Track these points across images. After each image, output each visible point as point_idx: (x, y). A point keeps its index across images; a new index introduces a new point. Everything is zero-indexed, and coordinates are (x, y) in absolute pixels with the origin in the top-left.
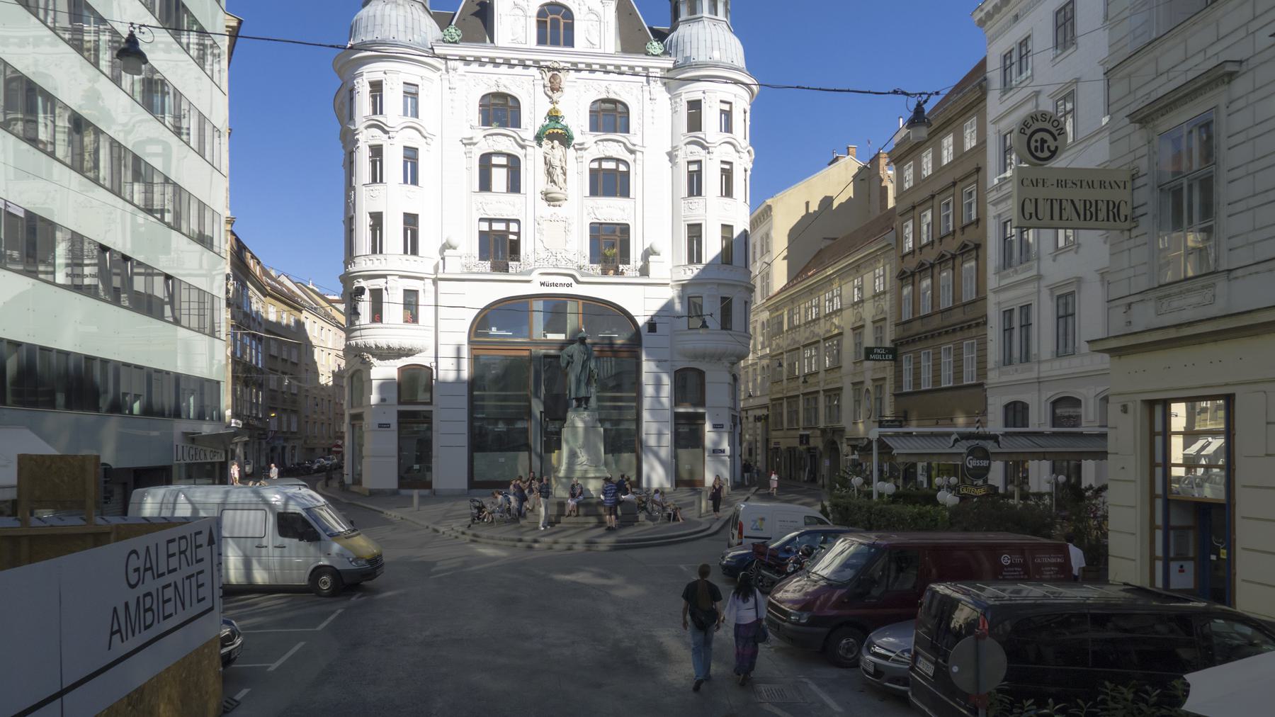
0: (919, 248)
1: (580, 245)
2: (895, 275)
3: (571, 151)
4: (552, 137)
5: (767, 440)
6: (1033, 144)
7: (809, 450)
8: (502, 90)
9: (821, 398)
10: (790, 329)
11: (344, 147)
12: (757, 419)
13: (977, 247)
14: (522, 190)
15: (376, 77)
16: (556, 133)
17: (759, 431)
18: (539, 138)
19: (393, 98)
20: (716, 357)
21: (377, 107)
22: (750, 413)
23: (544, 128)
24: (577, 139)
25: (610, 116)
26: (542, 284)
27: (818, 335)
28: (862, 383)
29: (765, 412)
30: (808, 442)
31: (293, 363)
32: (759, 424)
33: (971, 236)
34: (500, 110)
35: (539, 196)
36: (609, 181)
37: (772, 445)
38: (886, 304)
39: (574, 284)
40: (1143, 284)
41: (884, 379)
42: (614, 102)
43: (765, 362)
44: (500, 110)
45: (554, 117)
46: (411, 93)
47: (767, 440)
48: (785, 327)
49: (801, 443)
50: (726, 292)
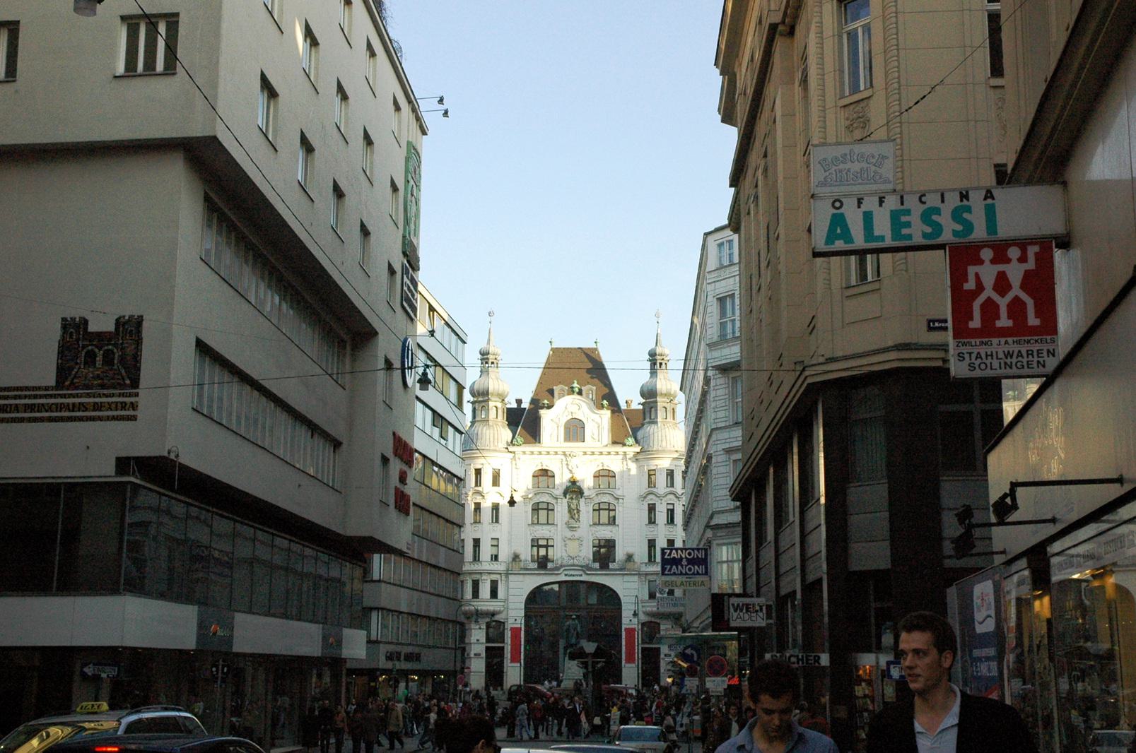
3: (582, 501)
15: (478, 467)
19: (487, 478)
21: (478, 482)
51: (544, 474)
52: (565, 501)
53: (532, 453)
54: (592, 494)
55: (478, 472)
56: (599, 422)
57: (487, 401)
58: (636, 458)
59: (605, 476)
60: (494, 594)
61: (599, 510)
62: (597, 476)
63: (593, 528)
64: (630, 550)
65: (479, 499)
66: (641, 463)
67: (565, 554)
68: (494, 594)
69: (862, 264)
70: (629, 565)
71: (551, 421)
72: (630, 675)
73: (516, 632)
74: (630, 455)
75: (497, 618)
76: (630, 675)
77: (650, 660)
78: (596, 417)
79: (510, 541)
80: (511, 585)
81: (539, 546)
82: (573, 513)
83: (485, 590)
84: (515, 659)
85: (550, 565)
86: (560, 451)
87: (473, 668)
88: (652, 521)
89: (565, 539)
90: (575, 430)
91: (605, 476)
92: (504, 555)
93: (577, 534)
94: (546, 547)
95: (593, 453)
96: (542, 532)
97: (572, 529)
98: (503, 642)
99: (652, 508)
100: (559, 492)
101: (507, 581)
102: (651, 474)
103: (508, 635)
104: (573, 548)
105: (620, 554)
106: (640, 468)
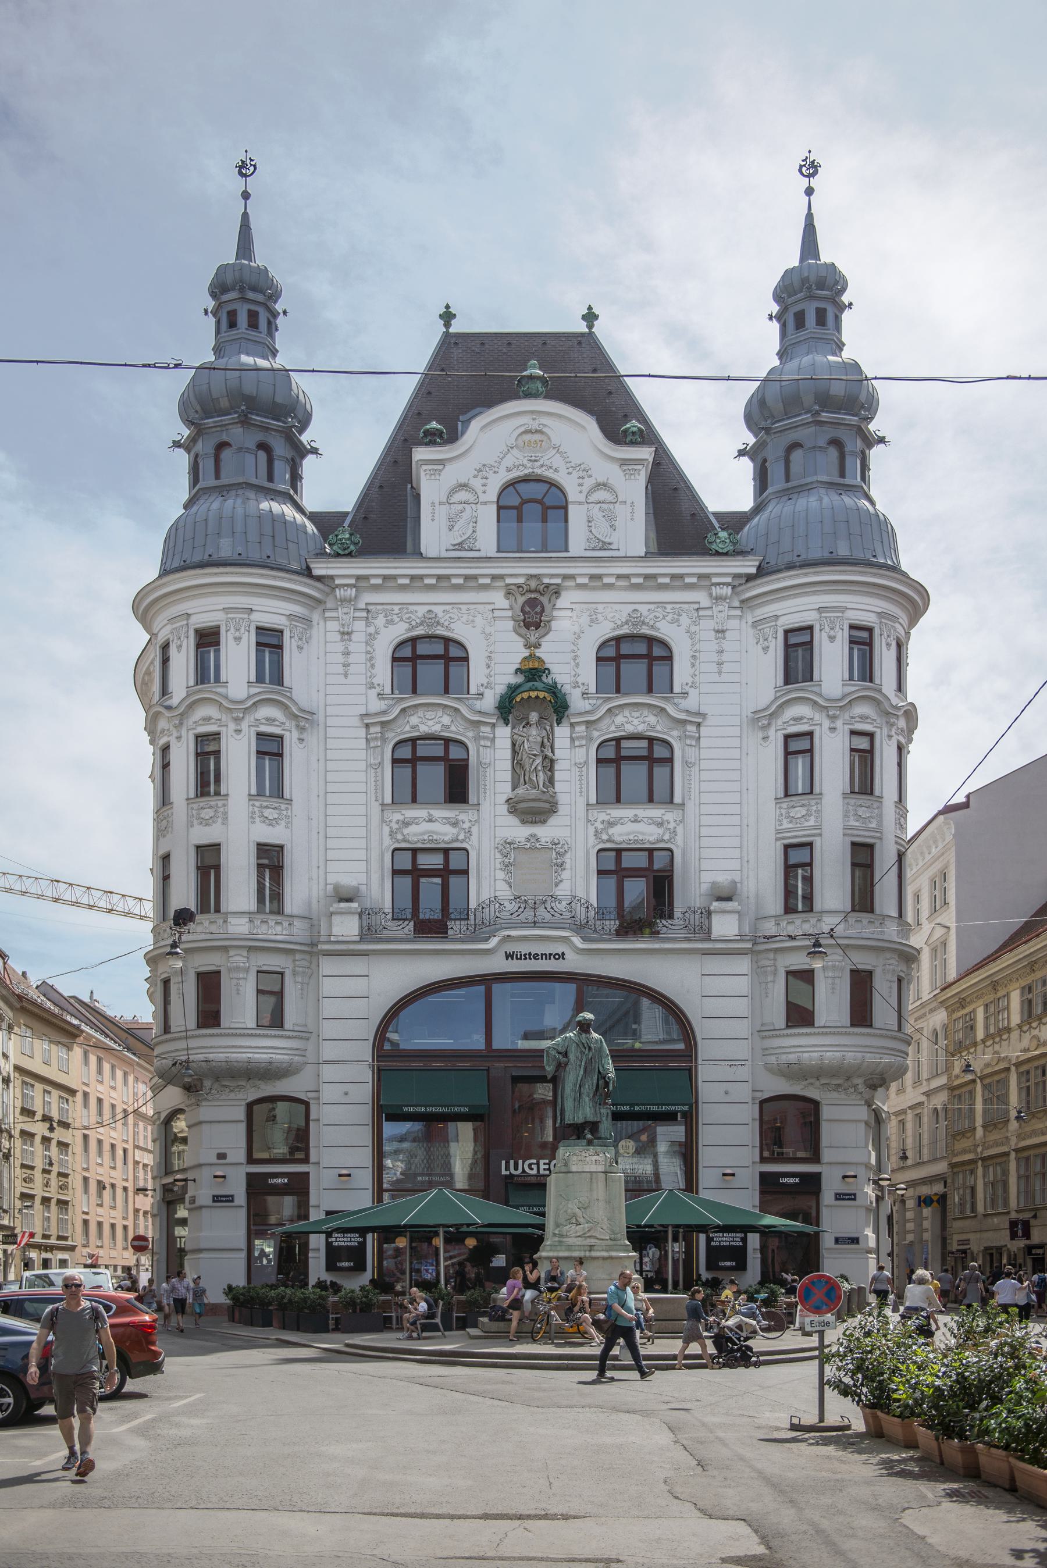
1: (580, 883)
3: (562, 733)
5: (944, 1241)
7: (1008, 1030)
10: (988, 1036)
11: (152, 742)
12: (924, 1201)
14: (472, 798)
16: (534, 698)
17: (926, 1224)
20: (839, 1076)
24: (577, 702)
25: (636, 659)
26: (509, 956)
29: (938, 1188)
30: (1027, 1235)
32: (927, 1212)
34: (429, 661)
35: (504, 809)
36: (638, 767)
37: (955, 1247)
43: (940, 1100)
44: (429, 661)
45: (533, 672)
46: (269, 643)
47: (944, 1241)
48: (980, 1034)
49: (1013, 1236)
50: (863, 961)
82: (533, 771)
83: (241, 1004)
100: (489, 702)
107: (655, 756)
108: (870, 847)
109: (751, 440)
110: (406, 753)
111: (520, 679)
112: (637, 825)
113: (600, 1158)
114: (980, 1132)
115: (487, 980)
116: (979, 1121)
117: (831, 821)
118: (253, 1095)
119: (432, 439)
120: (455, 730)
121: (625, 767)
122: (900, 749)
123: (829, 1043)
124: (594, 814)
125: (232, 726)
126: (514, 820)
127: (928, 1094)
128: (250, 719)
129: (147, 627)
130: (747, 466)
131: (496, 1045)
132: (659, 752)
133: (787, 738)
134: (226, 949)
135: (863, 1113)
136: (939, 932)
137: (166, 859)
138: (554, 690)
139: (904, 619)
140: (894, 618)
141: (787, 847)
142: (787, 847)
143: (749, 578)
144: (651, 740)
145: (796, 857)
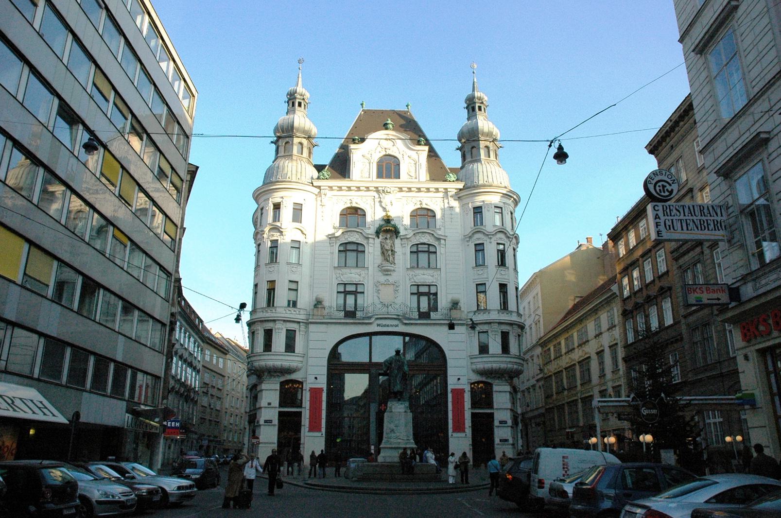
0: (634, 294)
2: (620, 312)
3: (397, 242)
4: (387, 231)
6: (658, 188)
8: (354, 205)
9: (580, 405)
13: (670, 289)
15: (277, 200)
18: (378, 233)
19: (286, 213)
21: (276, 218)
22: (533, 421)
23: (381, 226)
26: (378, 325)
27: (573, 360)
28: (606, 390)
30: (572, 437)
31: (218, 389)
33: (665, 283)
38: (617, 332)
39: (400, 325)
40: (743, 271)
41: (620, 385)
42: (428, 210)
49: (568, 438)
50: (505, 328)
51: (352, 215)
52: (378, 241)
53: (340, 189)
54: (410, 234)
55: (277, 207)
56: (413, 160)
57: (292, 137)
58: (458, 196)
59: (423, 215)
60: (290, 347)
61: (417, 252)
62: (414, 215)
63: (411, 273)
64: (456, 297)
65: (276, 236)
66: (465, 201)
67: (377, 301)
68: (290, 347)
69: (429, 300)
70: (455, 314)
71: (364, 157)
72: (460, 444)
73: (315, 393)
74: (453, 192)
75: (294, 377)
76: (460, 444)
77: (483, 428)
78: (413, 154)
79: (311, 286)
80: (312, 336)
81: (346, 293)
82: (387, 254)
83: (279, 341)
84: (314, 426)
85: (359, 314)
86: (372, 185)
87: (262, 438)
88: (480, 264)
89: (377, 284)
90: (389, 167)
91: (423, 215)
92: (305, 299)
93: (391, 279)
94: (355, 293)
95: (410, 190)
96: (352, 275)
97: (386, 272)
98: (301, 406)
99: (479, 248)
100: (372, 231)
101: (307, 332)
102: (478, 210)
103: (306, 399)
104: (387, 294)
105: (443, 302)
106: (462, 206)
107: (430, 251)
108: (506, 285)
109: (460, 145)
110: (415, 249)
111: (383, 223)
112: (424, 276)
113: (403, 406)
114: (579, 388)
115: (370, 335)
116: (579, 382)
117: (492, 275)
118: (282, 379)
119: (354, 141)
120: (360, 240)
121: (420, 255)
122: (514, 249)
123: (495, 360)
124: (409, 272)
125: (488, 240)
126: (380, 274)
127: (538, 381)
128: (494, 238)
129: (257, 203)
130: (459, 153)
131: (373, 361)
132: (432, 249)
133: (476, 245)
134: (274, 321)
135: (508, 388)
136: (537, 317)
137: (256, 286)
138: (395, 227)
139: (513, 205)
140: (509, 205)
141: (477, 285)
142: (477, 285)
143: (460, 190)
144: (429, 245)
145: (481, 288)
